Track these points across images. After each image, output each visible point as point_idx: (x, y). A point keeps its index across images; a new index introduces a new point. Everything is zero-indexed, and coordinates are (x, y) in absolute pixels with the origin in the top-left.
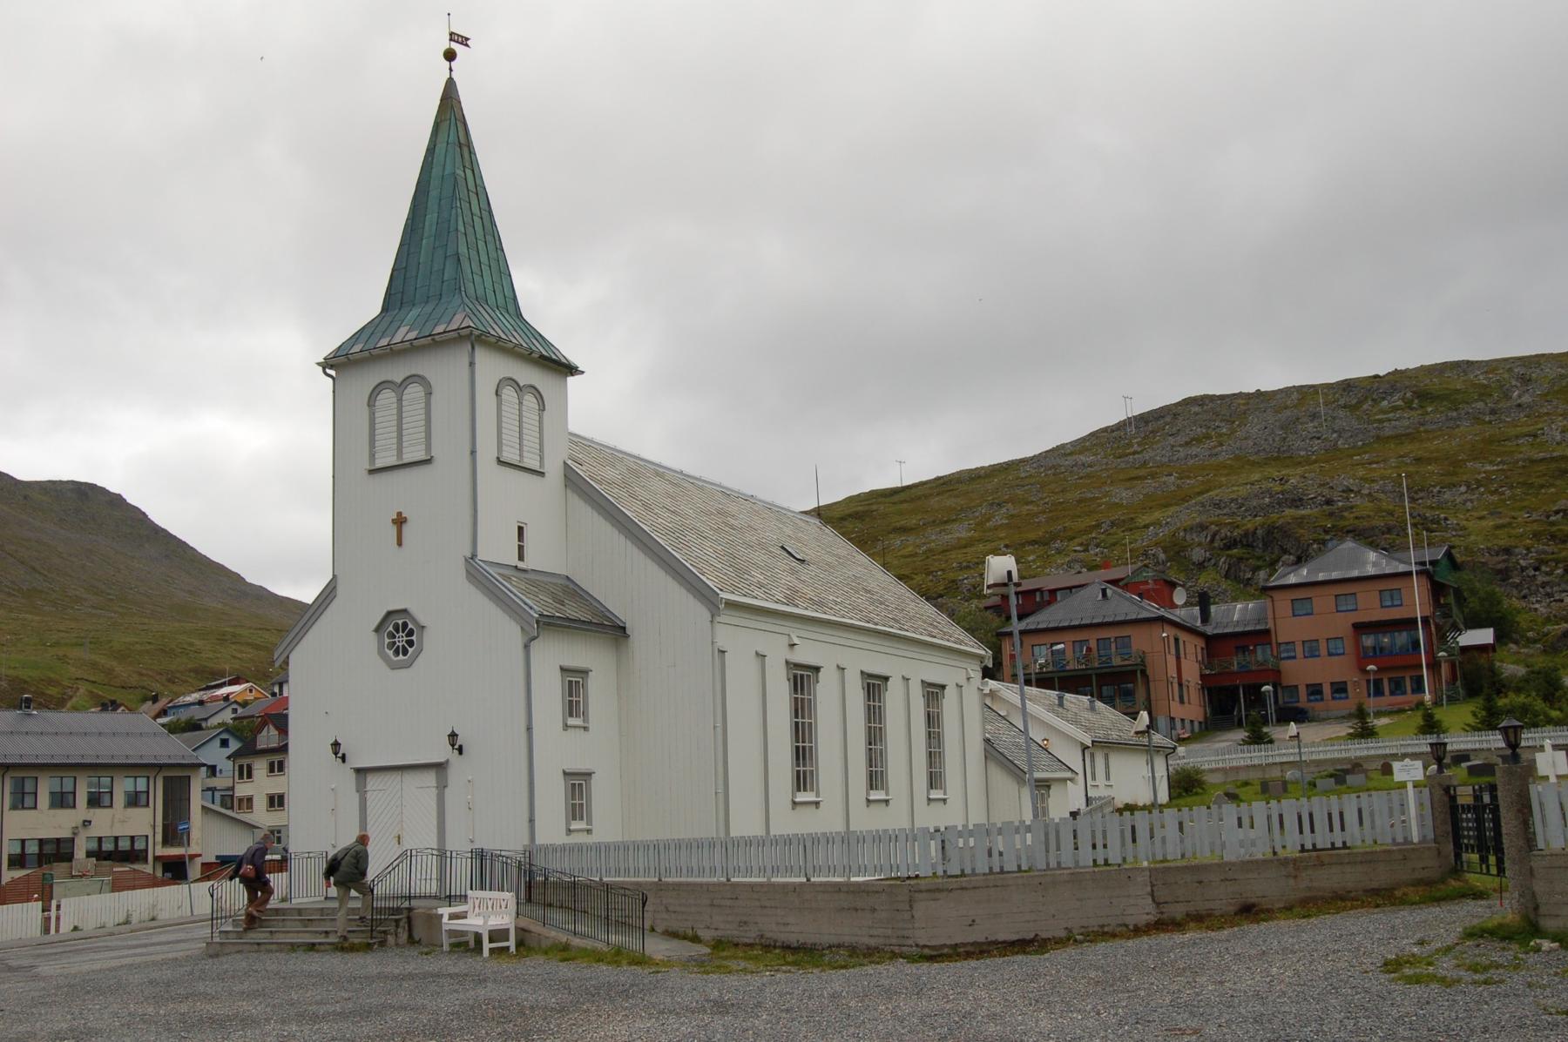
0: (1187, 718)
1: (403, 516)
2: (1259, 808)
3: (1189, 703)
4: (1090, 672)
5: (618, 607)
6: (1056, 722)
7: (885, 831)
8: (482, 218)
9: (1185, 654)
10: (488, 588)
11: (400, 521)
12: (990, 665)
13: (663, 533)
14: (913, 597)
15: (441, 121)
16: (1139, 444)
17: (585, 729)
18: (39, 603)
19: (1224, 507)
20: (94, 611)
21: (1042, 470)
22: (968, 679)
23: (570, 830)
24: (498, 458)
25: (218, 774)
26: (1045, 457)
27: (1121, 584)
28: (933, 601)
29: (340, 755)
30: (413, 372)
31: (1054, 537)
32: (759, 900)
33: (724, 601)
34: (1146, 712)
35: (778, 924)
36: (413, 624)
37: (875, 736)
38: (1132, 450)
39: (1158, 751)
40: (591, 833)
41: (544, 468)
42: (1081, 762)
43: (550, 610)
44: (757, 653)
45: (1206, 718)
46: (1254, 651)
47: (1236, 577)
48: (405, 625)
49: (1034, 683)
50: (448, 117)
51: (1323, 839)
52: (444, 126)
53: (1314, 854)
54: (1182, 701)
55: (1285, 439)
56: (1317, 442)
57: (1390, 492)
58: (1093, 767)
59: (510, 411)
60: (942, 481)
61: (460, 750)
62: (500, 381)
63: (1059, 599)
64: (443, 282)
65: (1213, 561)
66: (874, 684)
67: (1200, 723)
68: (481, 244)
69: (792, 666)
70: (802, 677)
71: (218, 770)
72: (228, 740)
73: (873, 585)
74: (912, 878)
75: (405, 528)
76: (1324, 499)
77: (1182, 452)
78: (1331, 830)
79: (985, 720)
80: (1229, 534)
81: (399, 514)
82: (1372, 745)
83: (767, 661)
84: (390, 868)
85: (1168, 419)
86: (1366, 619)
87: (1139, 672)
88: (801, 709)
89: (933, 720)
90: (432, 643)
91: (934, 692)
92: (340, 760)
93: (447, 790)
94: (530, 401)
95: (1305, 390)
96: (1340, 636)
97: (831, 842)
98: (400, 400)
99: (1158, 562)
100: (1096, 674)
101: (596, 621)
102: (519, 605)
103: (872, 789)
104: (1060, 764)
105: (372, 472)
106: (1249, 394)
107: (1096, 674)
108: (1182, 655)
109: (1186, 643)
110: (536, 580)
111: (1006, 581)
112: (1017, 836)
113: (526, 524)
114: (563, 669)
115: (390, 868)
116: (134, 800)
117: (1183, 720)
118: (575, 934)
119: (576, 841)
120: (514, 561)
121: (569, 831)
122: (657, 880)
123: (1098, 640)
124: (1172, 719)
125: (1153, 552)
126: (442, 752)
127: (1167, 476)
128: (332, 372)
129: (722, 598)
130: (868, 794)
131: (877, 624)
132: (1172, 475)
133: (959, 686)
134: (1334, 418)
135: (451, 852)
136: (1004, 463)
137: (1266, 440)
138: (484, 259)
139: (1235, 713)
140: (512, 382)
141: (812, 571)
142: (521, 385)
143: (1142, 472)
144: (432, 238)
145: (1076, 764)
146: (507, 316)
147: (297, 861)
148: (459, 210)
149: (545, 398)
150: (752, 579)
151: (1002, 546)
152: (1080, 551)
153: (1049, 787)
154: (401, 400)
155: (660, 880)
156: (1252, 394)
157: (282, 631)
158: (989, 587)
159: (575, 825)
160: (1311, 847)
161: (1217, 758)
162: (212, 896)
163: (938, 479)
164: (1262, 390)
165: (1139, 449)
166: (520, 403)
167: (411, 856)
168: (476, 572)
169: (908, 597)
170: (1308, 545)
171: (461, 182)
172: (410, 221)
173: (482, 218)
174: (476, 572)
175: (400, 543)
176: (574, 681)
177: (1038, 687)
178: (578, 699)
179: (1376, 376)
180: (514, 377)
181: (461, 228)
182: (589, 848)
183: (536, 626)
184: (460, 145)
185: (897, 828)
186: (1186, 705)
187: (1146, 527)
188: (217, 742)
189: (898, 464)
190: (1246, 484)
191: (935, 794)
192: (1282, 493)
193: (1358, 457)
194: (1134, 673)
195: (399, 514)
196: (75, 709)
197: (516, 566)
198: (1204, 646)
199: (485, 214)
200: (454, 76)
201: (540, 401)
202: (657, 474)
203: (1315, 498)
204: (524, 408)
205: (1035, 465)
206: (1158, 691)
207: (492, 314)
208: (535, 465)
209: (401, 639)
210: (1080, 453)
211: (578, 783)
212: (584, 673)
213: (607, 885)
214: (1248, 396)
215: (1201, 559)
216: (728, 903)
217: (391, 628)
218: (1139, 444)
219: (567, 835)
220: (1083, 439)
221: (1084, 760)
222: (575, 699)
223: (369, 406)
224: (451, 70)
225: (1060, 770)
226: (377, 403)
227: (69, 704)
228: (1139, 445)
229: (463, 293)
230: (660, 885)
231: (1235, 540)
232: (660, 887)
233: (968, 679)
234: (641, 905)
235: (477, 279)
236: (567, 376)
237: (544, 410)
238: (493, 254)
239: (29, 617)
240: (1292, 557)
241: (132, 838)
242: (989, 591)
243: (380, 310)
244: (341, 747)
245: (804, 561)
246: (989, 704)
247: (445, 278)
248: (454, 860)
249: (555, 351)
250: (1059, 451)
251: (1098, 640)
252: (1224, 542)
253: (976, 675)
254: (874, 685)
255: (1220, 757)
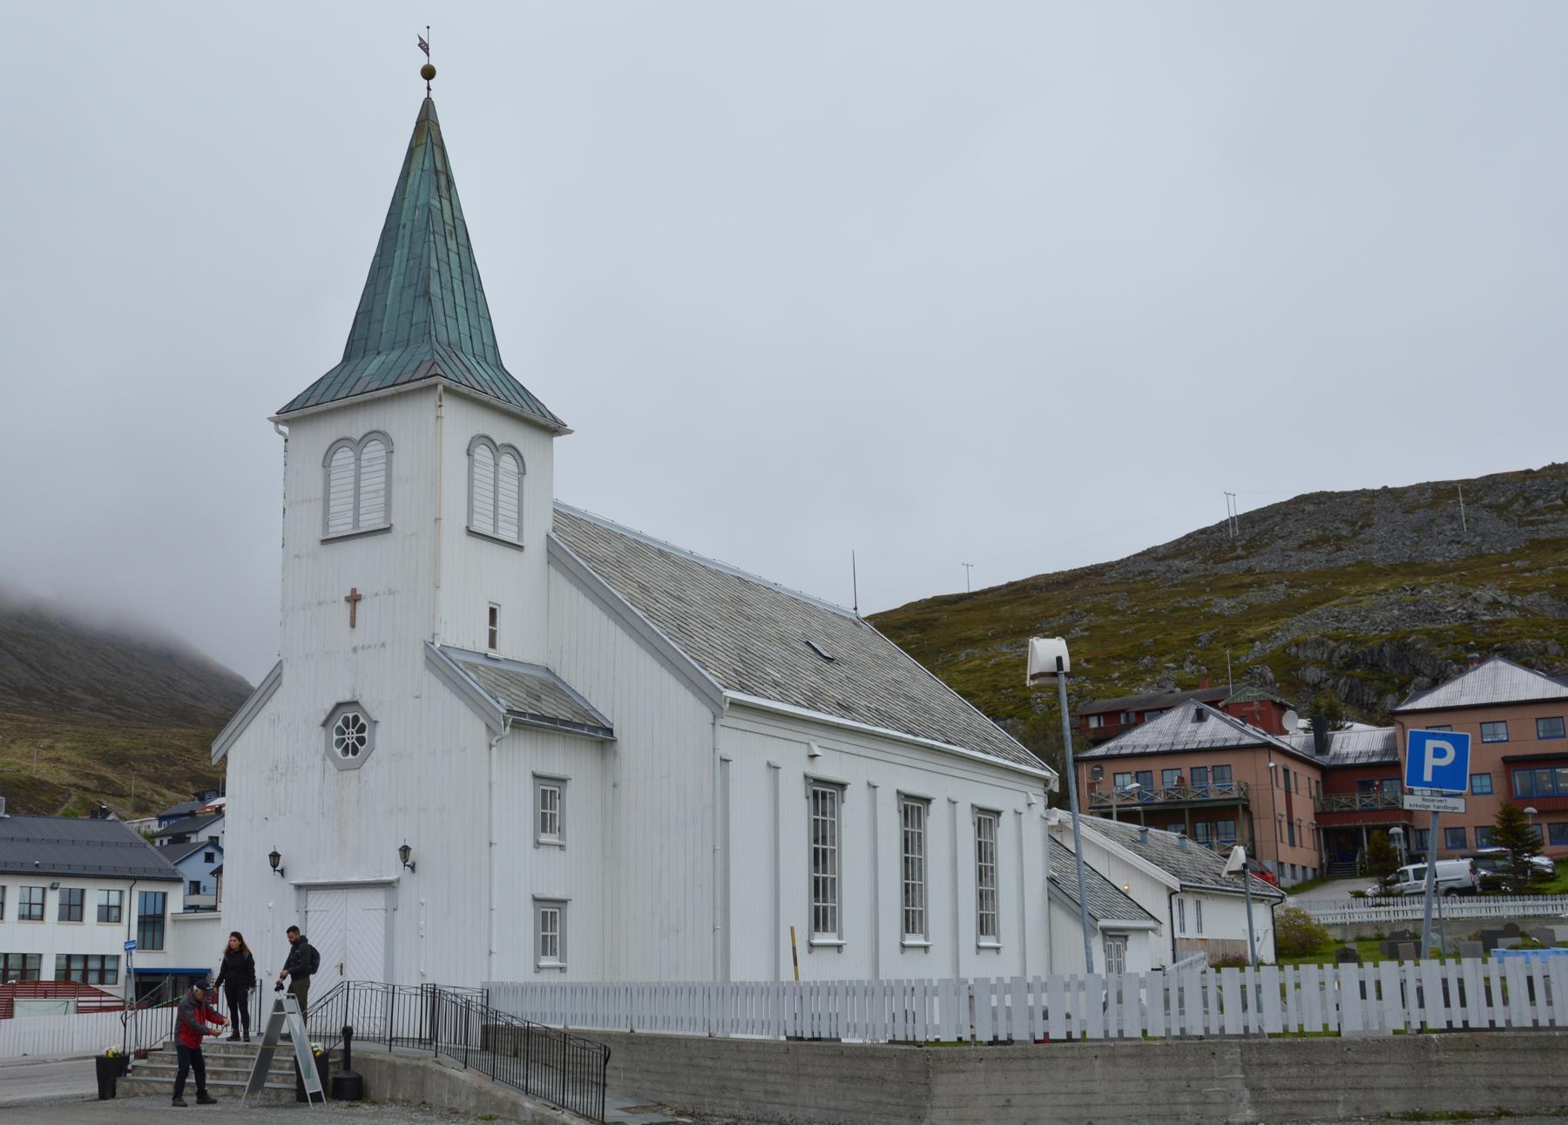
0: (1299, 863)
1: (358, 593)
2: (1388, 971)
3: (1301, 846)
4: (1180, 807)
5: (604, 705)
6: (1153, 870)
7: (898, 982)
8: (459, 254)
9: (1297, 789)
10: (458, 686)
11: (354, 599)
12: (1056, 789)
13: (661, 620)
14: (964, 707)
15: (416, 146)
16: (1244, 547)
17: (561, 847)
18: (36, 703)
19: (1345, 620)
20: (91, 713)
21: (1130, 576)
22: (1029, 805)
23: (538, 967)
24: (467, 527)
25: (201, 891)
26: (1134, 563)
27: (1220, 705)
28: (1002, 723)
29: (279, 868)
30: (374, 428)
31: (1142, 651)
32: (745, 1062)
33: (728, 700)
34: (1241, 848)
35: (766, 1092)
36: (366, 720)
37: (912, 867)
38: (1235, 554)
39: (1263, 900)
40: (565, 972)
41: (522, 541)
42: (1168, 911)
43: (521, 705)
44: (769, 764)
45: (1321, 865)
46: (1380, 787)
47: (1358, 701)
48: (356, 719)
49: (1115, 816)
50: (424, 142)
51: (1478, 1015)
52: (419, 152)
53: (1466, 1035)
54: (1292, 844)
55: (1417, 543)
56: (1456, 546)
57: (1548, 605)
58: (1182, 917)
59: (484, 472)
60: (1014, 587)
61: (413, 868)
62: (473, 438)
63: (1146, 720)
64: (411, 325)
65: (1330, 682)
66: (913, 807)
67: (1314, 870)
68: (457, 283)
69: (812, 781)
70: (824, 794)
71: (201, 886)
72: (212, 854)
73: (916, 691)
74: (932, 1043)
75: (359, 606)
76: (1464, 612)
77: (1295, 556)
78: (1490, 1003)
79: (1051, 856)
80: (1350, 650)
81: (354, 590)
82: (1530, 902)
83: (781, 775)
84: (322, 1002)
85: (1278, 519)
86: (1520, 752)
87: (1240, 808)
88: (911, 843)
89: (984, 852)
90: (383, 739)
91: (986, 818)
92: (280, 874)
93: (398, 914)
94: (508, 462)
95: (1442, 487)
96: (1486, 772)
97: (832, 993)
98: (358, 460)
99: (1266, 683)
100: (1190, 809)
101: (577, 721)
102: (484, 698)
103: (907, 931)
104: (1140, 911)
105: (325, 542)
106: (1373, 491)
107: (1190, 809)
108: (1293, 790)
109: (1298, 775)
110: (507, 675)
111: (1056, 670)
112: (1068, 994)
113: (499, 606)
114: (536, 776)
115: (322, 1002)
116: (108, 914)
117: (1293, 866)
118: (527, 1094)
119: (546, 980)
120: (483, 646)
121: (538, 968)
122: (628, 1030)
123: (1191, 769)
124: (1281, 864)
125: (1259, 671)
126: (392, 869)
127: (1276, 583)
128: (285, 429)
129: (726, 697)
130: (903, 938)
131: (917, 735)
132: (1282, 583)
133: (1018, 814)
134: (1477, 520)
135: (349, 982)
136: (1087, 568)
137: (1394, 544)
138: (460, 299)
139: (1357, 860)
140: (487, 440)
141: (843, 672)
142: (498, 444)
143: (1247, 580)
144: (402, 277)
145: (1160, 910)
146: (484, 364)
147: (357, 993)
148: (432, 245)
149: (525, 460)
150: (766, 677)
151: (1082, 661)
152: (1173, 669)
153: (1126, 937)
154: (360, 459)
155: (632, 1031)
156: (1377, 491)
157: (220, 722)
158: (1033, 677)
159: (545, 962)
160: (1461, 1026)
161: (1334, 912)
162: (125, 1025)
163: (1010, 584)
164: (1389, 487)
165: (1244, 553)
166: (496, 465)
167: (348, 989)
168: (439, 661)
169: (960, 708)
170: (1446, 666)
171: (436, 212)
172: (377, 258)
173: (459, 254)
174: (439, 661)
175: (353, 625)
176: (549, 790)
177: (1119, 819)
178: (553, 812)
179: (1529, 472)
180: (492, 436)
181: (434, 264)
182: (563, 989)
183: (503, 723)
184: (436, 172)
185: (893, 978)
186: (1298, 848)
187: (1252, 641)
188: (201, 856)
189: (965, 567)
190: (1372, 594)
191: (987, 941)
192: (1415, 603)
193: (1506, 565)
194: (1234, 809)
195: (354, 590)
196: (65, 816)
197: (486, 655)
198: (1319, 780)
199: (463, 251)
200: (432, 95)
201: (521, 465)
202: (661, 553)
203: (1454, 610)
204: (501, 471)
205: (1122, 571)
206: (1263, 830)
207: (467, 363)
208: (512, 538)
209: (351, 736)
210: (1175, 556)
211: (549, 912)
212: (563, 781)
213: (565, 1034)
214: (1373, 494)
215: (1316, 680)
216: (709, 1063)
217: (340, 723)
218: (1244, 547)
219: (535, 972)
220: (1179, 542)
221: (1171, 908)
222: (548, 811)
223: (324, 467)
224: (429, 89)
225: (1141, 918)
226: (333, 464)
227: (61, 811)
228: (1243, 549)
229: (434, 338)
230: (632, 1037)
231: (1357, 657)
232: (632, 1040)
233: (1029, 805)
234: (603, 1063)
235: (451, 323)
236: (553, 436)
237: (524, 474)
238: (470, 295)
239: (25, 717)
240: (1426, 679)
241: (103, 958)
242: (1032, 683)
243: (340, 360)
244: (281, 858)
245: (833, 660)
246: (1053, 838)
247: (414, 322)
248: (396, 996)
249: (540, 407)
250: (1152, 554)
251: (1191, 769)
252: (1345, 660)
253: (1040, 802)
254: (913, 807)
255: (1338, 911)
